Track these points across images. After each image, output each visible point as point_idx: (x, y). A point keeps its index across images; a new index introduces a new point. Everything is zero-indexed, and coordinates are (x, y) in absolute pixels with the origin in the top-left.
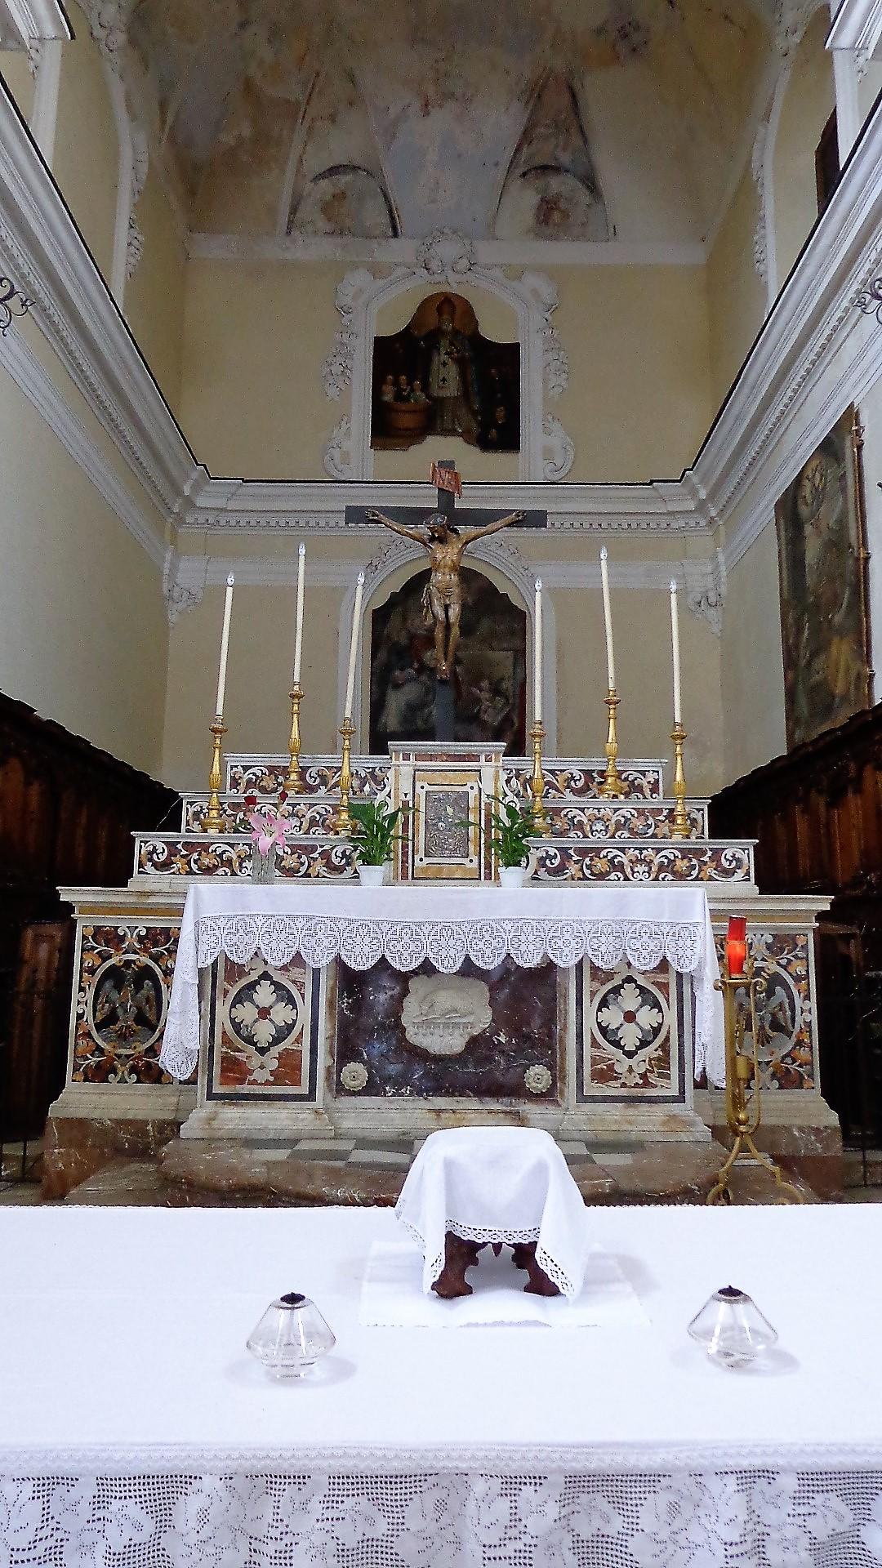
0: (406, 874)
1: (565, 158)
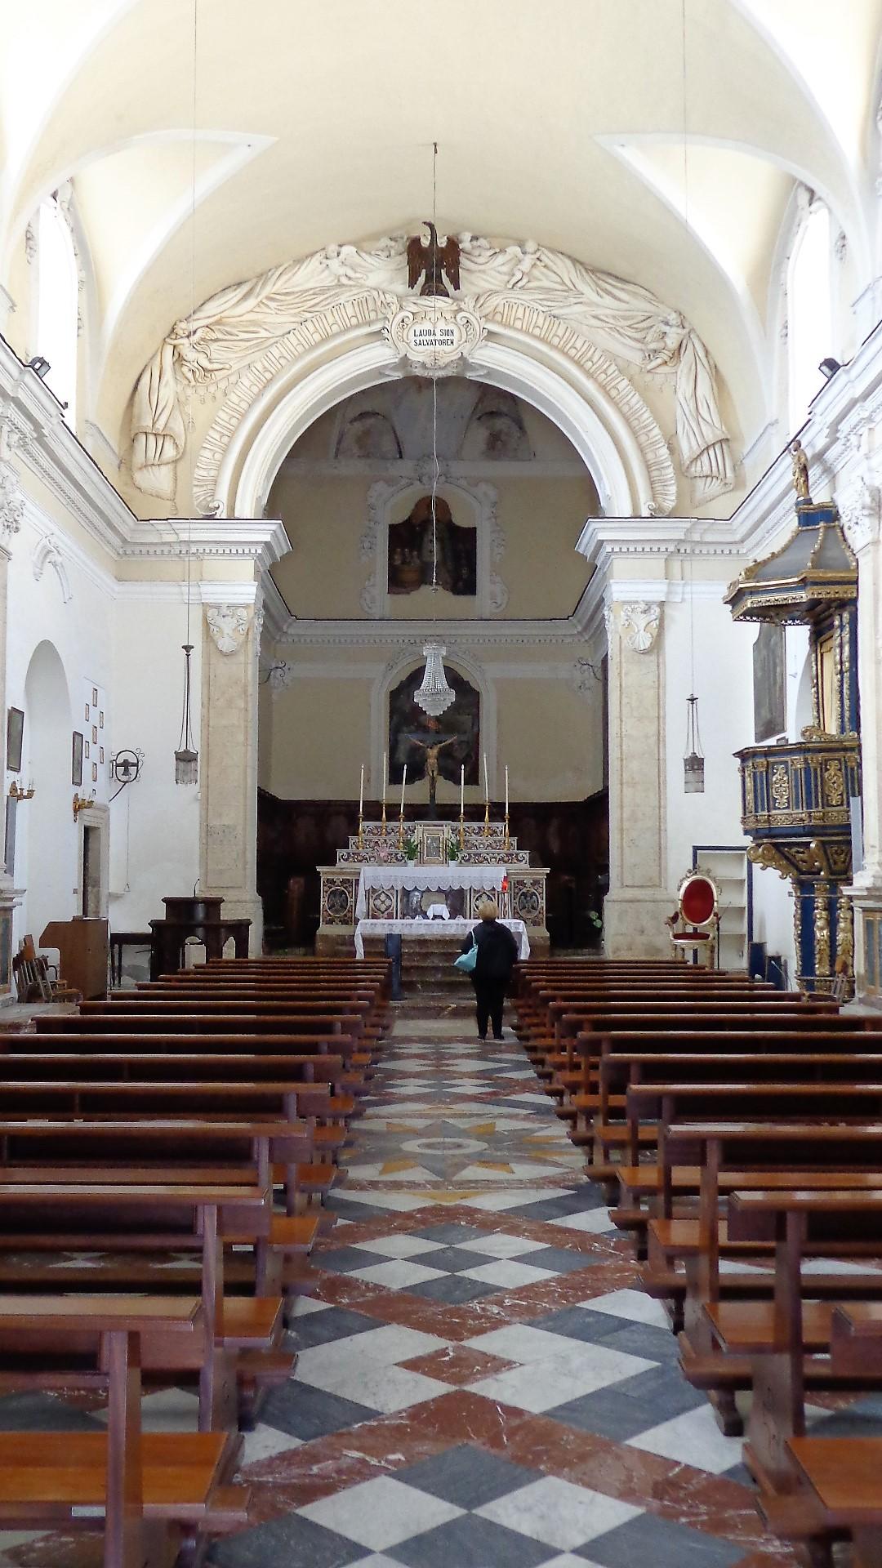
0: (421, 863)
1: (505, 409)
